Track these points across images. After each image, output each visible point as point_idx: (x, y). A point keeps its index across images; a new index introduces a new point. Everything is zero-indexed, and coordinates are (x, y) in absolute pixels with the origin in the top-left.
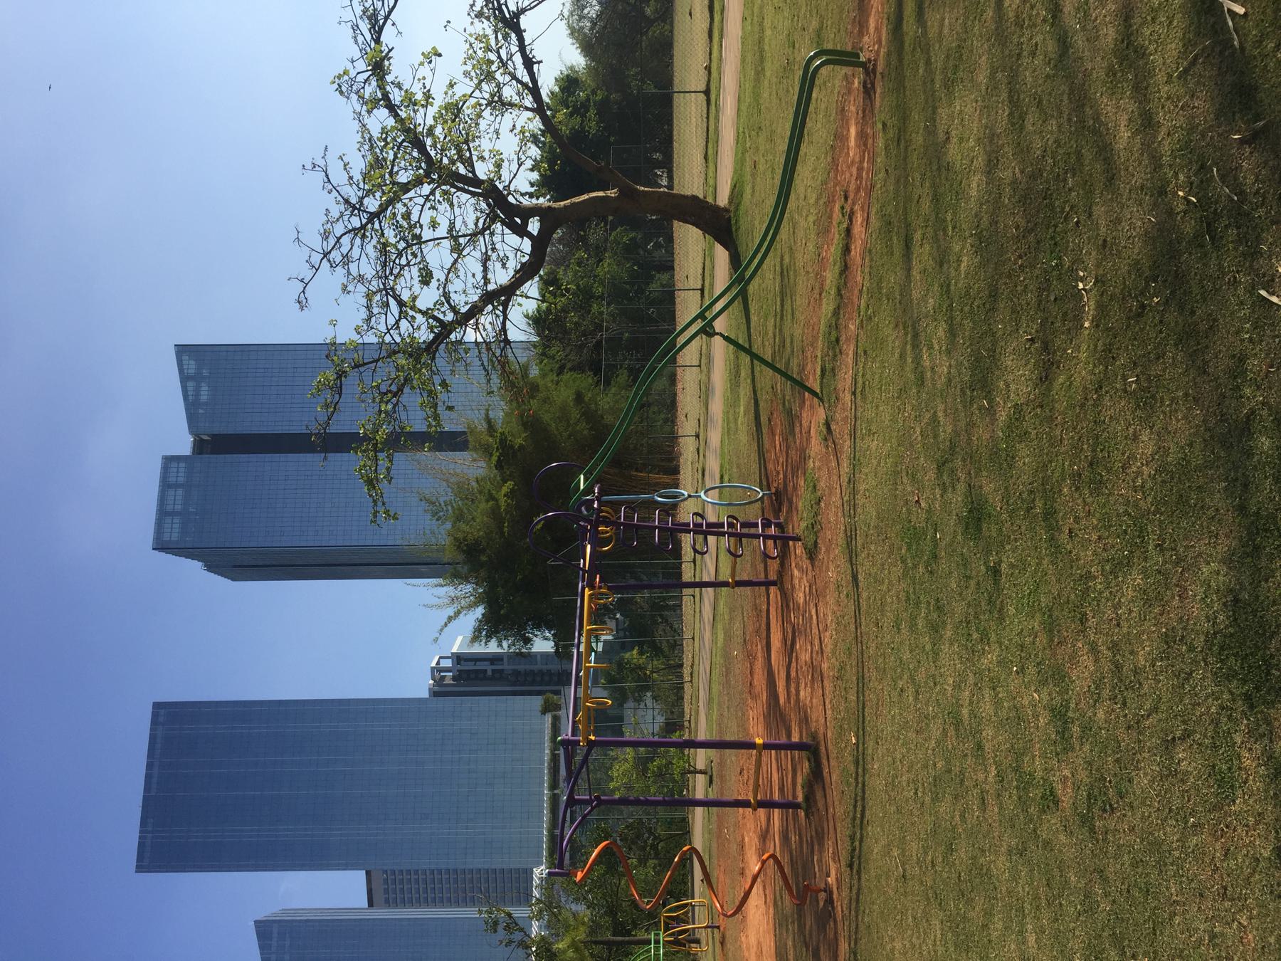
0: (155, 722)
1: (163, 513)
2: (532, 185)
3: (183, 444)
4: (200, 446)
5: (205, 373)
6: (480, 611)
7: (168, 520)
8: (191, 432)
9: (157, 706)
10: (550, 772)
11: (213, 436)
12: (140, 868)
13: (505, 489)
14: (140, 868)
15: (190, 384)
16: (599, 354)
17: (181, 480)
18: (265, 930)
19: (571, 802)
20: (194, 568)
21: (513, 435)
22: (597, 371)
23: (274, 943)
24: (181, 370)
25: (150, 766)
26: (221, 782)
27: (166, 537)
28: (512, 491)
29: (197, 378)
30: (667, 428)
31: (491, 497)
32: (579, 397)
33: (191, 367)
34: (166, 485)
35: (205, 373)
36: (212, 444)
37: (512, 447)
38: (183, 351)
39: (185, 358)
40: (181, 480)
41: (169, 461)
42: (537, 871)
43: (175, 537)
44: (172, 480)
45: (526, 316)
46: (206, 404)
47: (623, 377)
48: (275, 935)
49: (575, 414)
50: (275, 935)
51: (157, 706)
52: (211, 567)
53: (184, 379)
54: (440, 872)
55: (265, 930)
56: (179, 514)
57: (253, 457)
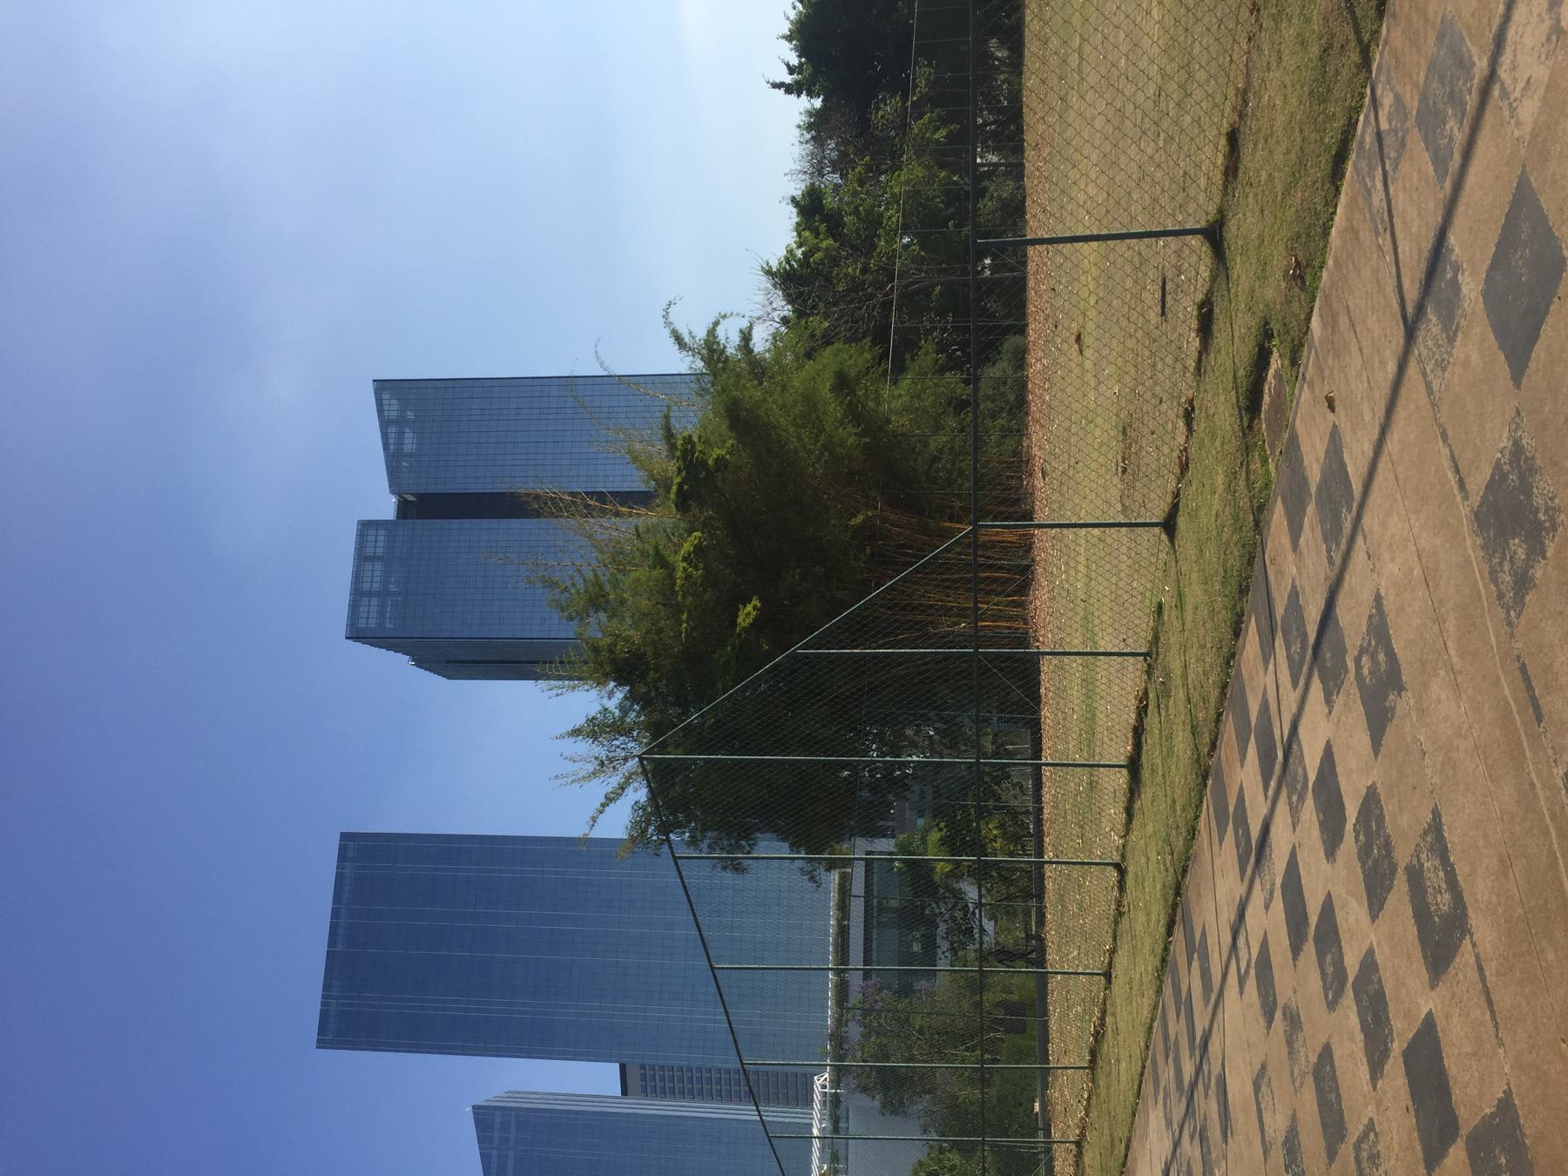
0: (342, 857)
1: (359, 594)
2: (791, 70)
3: (386, 507)
4: (404, 509)
5: (410, 415)
6: (639, 793)
7: (365, 601)
8: (393, 492)
9: (345, 837)
10: (836, 951)
11: (420, 496)
12: (322, 1043)
13: (687, 547)
14: (322, 1043)
15: (392, 430)
16: (888, 317)
17: (380, 551)
18: (485, 1117)
19: (881, 910)
20: (400, 663)
21: (707, 442)
22: (880, 336)
23: (496, 1135)
24: (380, 411)
25: (335, 913)
26: (421, 939)
27: (362, 623)
28: (699, 550)
29: (400, 422)
30: (1010, 443)
31: (661, 561)
32: (843, 383)
33: (393, 408)
34: (362, 558)
35: (410, 415)
36: (420, 506)
37: (704, 463)
38: (384, 388)
39: (386, 396)
40: (380, 551)
41: (366, 527)
42: (818, 1082)
43: (373, 623)
44: (369, 551)
45: (769, 272)
46: (411, 455)
47: (928, 355)
48: (497, 1126)
49: (833, 409)
50: (497, 1126)
51: (345, 837)
52: (420, 663)
53: (384, 424)
54: (690, 1070)
55: (485, 1117)
56: (377, 594)
57: (466, 523)
